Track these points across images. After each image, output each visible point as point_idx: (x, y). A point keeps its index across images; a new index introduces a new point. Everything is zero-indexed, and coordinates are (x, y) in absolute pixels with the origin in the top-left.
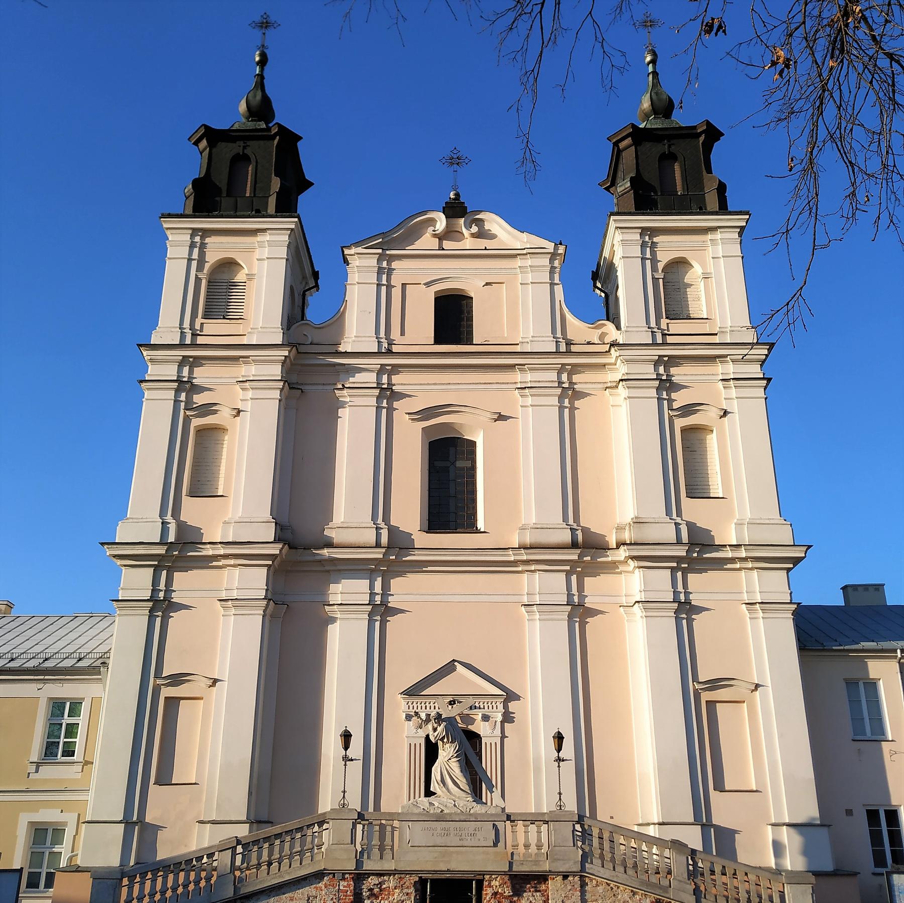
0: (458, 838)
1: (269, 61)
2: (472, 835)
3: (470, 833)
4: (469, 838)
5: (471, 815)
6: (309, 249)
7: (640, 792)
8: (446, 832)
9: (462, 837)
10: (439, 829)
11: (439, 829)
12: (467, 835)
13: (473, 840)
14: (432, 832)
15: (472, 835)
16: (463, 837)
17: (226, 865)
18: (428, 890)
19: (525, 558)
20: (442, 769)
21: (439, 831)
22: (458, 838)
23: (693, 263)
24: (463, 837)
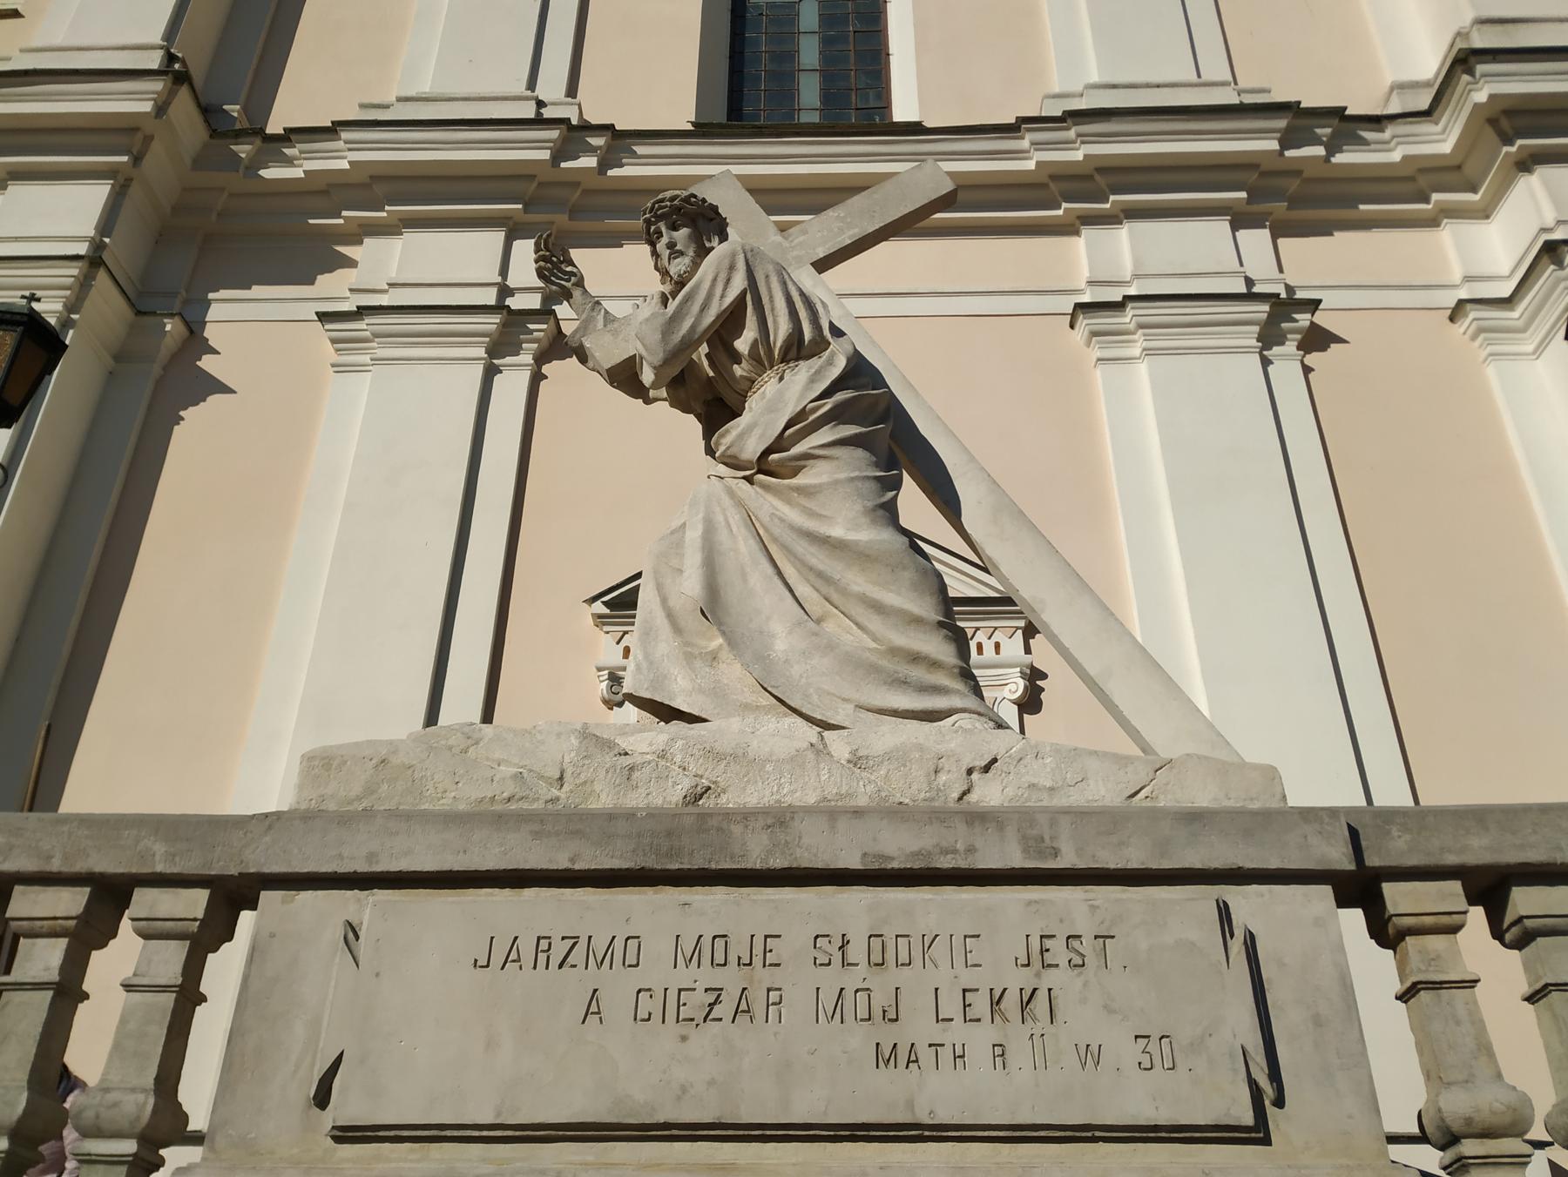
0: (858, 1039)
1: (105, 949)
2: (1011, 1003)
3: (983, 980)
4: (979, 1039)
5: (979, 818)
6: (380, 305)
7: (533, 1131)
8: (732, 980)
9: (903, 1034)
10: (657, 948)
11: (657, 948)
12: (950, 1007)
13: (1020, 1054)
14: (575, 983)
15: (1011, 1003)
16: (918, 1028)
17: (1448, 973)
18: (26, 453)
19: (731, 521)
20: (723, 536)
21: (658, 971)
22: (858, 1039)
23: (1083, 236)
24: (918, 1028)
